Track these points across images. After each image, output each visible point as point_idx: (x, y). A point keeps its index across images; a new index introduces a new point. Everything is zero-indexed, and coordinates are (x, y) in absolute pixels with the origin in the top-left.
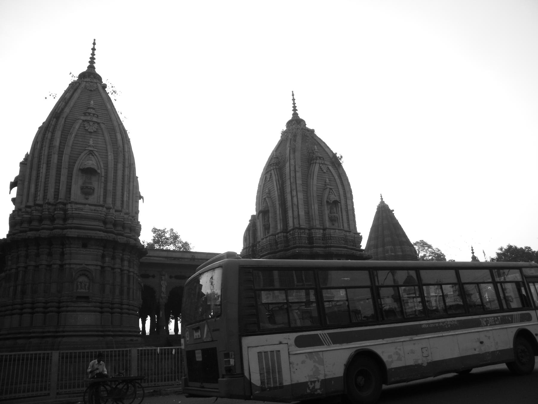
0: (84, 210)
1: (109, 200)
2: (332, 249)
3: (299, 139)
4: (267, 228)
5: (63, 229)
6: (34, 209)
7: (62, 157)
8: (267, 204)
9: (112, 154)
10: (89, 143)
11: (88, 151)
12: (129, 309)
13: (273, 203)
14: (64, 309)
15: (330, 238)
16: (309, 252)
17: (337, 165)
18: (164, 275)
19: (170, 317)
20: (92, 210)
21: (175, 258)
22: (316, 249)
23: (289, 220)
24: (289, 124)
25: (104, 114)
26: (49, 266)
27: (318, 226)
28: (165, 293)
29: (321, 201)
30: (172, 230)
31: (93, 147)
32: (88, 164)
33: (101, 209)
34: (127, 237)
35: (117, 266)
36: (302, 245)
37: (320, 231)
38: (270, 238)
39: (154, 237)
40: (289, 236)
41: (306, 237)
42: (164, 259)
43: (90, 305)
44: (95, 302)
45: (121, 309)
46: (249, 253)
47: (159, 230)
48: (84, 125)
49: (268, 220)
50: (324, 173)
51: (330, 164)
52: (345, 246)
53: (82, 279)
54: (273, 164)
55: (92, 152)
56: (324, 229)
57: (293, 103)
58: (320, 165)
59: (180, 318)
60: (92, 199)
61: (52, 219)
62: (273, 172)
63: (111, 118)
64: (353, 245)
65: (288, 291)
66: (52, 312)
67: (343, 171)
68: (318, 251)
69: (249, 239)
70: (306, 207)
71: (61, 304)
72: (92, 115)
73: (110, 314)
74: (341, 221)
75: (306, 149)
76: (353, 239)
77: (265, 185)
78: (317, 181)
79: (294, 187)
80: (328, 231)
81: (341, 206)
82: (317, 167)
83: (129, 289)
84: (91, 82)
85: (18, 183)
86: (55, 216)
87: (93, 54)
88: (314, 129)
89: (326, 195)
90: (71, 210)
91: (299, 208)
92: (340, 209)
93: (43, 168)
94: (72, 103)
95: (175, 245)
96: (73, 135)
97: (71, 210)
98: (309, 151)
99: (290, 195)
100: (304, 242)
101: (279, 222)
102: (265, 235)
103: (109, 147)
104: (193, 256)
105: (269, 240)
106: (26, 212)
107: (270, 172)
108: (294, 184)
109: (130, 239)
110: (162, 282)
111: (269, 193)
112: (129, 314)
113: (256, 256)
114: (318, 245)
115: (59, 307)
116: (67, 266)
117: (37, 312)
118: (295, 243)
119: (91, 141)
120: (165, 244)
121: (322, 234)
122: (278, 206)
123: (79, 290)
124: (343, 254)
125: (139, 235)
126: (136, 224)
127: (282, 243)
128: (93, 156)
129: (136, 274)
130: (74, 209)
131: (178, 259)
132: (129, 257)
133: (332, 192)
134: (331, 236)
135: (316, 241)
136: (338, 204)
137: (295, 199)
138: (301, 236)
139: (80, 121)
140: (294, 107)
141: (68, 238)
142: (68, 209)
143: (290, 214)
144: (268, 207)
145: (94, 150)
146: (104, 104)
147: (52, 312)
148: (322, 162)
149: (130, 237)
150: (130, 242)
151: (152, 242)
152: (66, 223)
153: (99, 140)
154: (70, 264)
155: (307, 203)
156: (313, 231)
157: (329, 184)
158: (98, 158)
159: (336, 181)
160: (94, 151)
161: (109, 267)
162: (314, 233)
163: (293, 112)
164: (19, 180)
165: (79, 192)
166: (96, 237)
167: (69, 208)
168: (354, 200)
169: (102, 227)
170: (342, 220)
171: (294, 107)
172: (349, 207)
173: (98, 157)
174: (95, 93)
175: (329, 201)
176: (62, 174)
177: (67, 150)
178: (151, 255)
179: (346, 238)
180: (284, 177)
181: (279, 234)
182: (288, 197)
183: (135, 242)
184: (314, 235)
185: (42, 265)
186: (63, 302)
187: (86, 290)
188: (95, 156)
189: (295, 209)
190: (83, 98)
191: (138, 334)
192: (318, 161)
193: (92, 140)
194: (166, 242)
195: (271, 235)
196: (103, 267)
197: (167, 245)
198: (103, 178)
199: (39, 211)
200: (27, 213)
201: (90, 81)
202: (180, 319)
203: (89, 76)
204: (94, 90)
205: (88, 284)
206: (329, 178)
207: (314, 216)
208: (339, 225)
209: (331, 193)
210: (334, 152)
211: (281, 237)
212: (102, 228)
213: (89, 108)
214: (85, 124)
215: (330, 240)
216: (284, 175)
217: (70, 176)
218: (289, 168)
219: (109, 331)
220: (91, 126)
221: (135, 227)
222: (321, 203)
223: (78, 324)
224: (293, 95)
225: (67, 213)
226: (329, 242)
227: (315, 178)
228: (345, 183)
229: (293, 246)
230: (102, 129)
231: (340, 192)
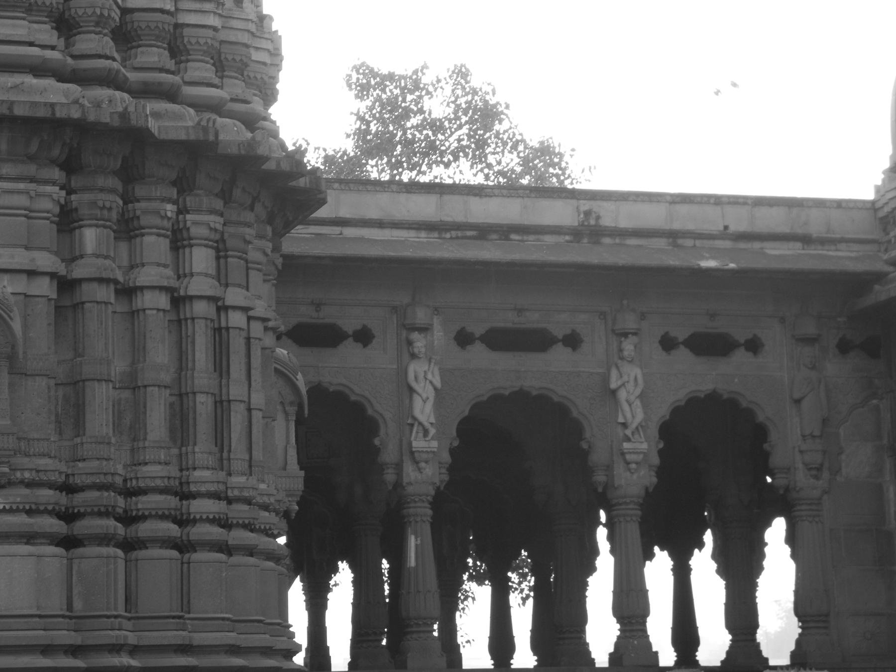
12: (225, 524)
18: (424, 329)
19: (466, 568)
21: (483, 232)
28: (432, 431)
30: (461, 73)
34: (199, 106)
35: (146, 276)
39: (361, 119)
42: (423, 234)
44: (30, 484)
47: (391, 77)
59: (523, 576)
65: (136, 195)
73: (120, 553)
83: (222, 405)
95: (481, 162)
104: (588, 214)
109: (220, 120)
110: (415, 369)
112: (227, 549)
120: (426, 155)
125: (269, 96)
126: (252, 27)
129: (264, 320)
131: (505, 231)
132: (216, 221)
149: (217, 108)
150: (221, 137)
151: (349, 146)
161: (101, 280)
166: (18, 111)
169: (53, 48)
178: (345, 213)
183: (249, 135)
191: (285, 665)
194: (432, 147)
197: (437, 163)
202: (520, 583)
212: (49, 54)
219: (115, 648)
221: (247, 46)
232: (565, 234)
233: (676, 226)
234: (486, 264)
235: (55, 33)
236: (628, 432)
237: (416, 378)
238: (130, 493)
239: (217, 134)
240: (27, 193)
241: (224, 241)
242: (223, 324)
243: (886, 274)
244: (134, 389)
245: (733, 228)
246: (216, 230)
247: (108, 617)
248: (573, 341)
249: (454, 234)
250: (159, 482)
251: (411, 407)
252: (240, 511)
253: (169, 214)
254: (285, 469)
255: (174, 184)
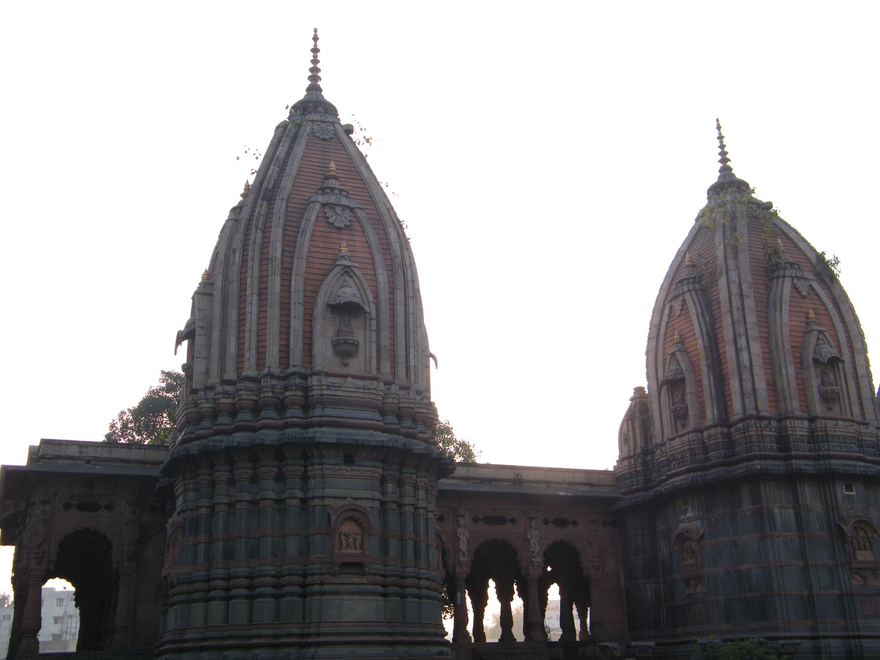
0: (343, 389)
1: (386, 366)
2: (833, 461)
3: (742, 224)
4: (680, 416)
5: (306, 427)
6: (243, 387)
7: (290, 280)
8: (679, 364)
9: (385, 272)
10: (340, 251)
11: (341, 267)
12: (419, 588)
13: (692, 363)
14: (316, 588)
15: (825, 439)
16: (784, 468)
17: (827, 280)
18: (463, 516)
20: (358, 388)
22: (798, 461)
23: (731, 400)
24: (715, 191)
25: (357, 189)
26: (280, 501)
27: (798, 413)
28: (466, 554)
29: (800, 358)
31: (350, 260)
32: (345, 295)
33: (375, 386)
36: (767, 453)
37: (803, 424)
38: (691, 437)
40: (734, 434)
41: (773, 436)
43: (365, 580)
44: (374, 574)
45: (402, 587)
46: (636, 468)
48: (326, 213)
49: (683, 400)
50: (804, 297)
51: (813, 278)
52: (861, 457)
53: (348, 527)
54: (688, 279)
55: (348, 270)
56: (812, 419)
57: (719, 144)
58: (793, 280)
60: (356, 365)
61: (281, 407)
62: (690, 298)
63: (371, 197)
64: (875, 453)
66: (292, 594)
67: (842, 292)
68: (803, 467)
69: (635, 438)
70: (769, 371)
71: (309, 579)
72: (337, 192)
74: (847, 402)
75: (762, 247)
76: (874, 440)
77: (670, 324)
78: (789, 315)
79: (742, 330)
80: (820, 423)
81: (844, 368)
82: (787, 285)
84: (323, 122)
85: (197, 333)
86: (286, 402)
87: (315, 61)
88: (772, 201)
89: (812, 347)
90: (319, 388)
91: (755, 373)
92: (842, 376)
93: (251, 303)
94: (293, 168)
96: (308, 235)
97: (319, 388)
98: (769, 252)
99: (733, 346)
100: (769, 447)
101: (708, 402)
102: (677, 431)
103: (378, 258)
105: (689, 442)
106: (223, 394)
107: (681, 298)
108: (742, 323)
111: (682, 341)
112: (419, 597)
113: (651, 474)
114: (801, 453)
115: (304, 586)
116: (317, 502)
117: (263, 595)
118: (749, 448)
119: (344, 247)
121: (807, 429)
122: (704, 370)
123: (343, 551)
124: (859, 473)
127: (719, 450)
128: (351, 277)
130: (325, 387)
132: (426, 480)
133: (824, 338)
134: (827, 435)
135: (796, 444)
136: (838, 365)
137: (745, 355)
138: (762, 435)
139: (318, 206)
140: (723, 154)
141: (319, 445)
142: (312, 387)
143: (734, 385)
144: (682, 371)
145: (353, 266)
146: (355, 167)
147: (292, 594)
148: (798, 275)
150: (433, 452)
152: (310, 414)
153: (357, 244)
154: (323, 498)
155: (771, 364)
156: (788, 422)
157: (815, 322)
158: (360, 281)
159: (829, 315)
160: (352, 268)
162: (792, 427)
163: (721, 165)
164: (198, 327)
165: (329, 351)
166: (372, 443)
167: (314, 384)
168: (869, 355)
169: (379, 421)
170: (849, 399)
171: (723, 154)
172: (861, 371)
173: (361, 279)
174: (333, 144)
175: (820, 358)
176: (292, 316)
177: (299, 267)
179: (860, 438)
180: (714, 307)
181: (711, 429)
182: (727, 350)
184: (790, 433)
185: (266, 499)
186: (313, 575)
187: (356, 549)
188: (354, 278)
189: (746, 376)
190: (313, 156)
192: (788, 273)
193: (345, 245)
195: (692, 432)
196: (383, 503)
198: (374, 323)
199: (250, 391)
200: (226, 394)
201: (320, 118)
203: (315, 109)
204: (331, 138)
205: (359, 537)
206: (815, 309)
207: (787, 391)
208: (843, 410)
209: (821, 342)
210: (818, 251)
211: (717, 435)
212: (379, 423)
213: (327, 178)
214: (326, 211)
215: (826, 444)
216: (714, 303)
217: (309, 320)
218: (726, 289)
220: (339, 215)
222: (801, 364)
223: (344, 620)
224: (719, 128)
225: (311, 394)
226: (823, 446)
227: (786, 309)
228: (848, 318)
229: (745, 455)
230: (359, 221)
231: (840, 338)
232: (511, 482)
233: (548, 479)
234: (487, 493)
235: (381, 416)
236: (534, 555)
237: (460, 534)
238: (403, 578)
239: (432, 451)
240: (372, 471)
241: (417, 484)
242: (417, 514)
243: (621, 498)
244: (402, 540)
245: (567, 480)
246: (426, 484)
247: (398, 622)
248: (513, 521)
249: (473, 481)
250: (412, 574)
251: (458, 545)
252: (424, 583)
253: (414, 478)
254: (438, 568)
255: (414, 467)
